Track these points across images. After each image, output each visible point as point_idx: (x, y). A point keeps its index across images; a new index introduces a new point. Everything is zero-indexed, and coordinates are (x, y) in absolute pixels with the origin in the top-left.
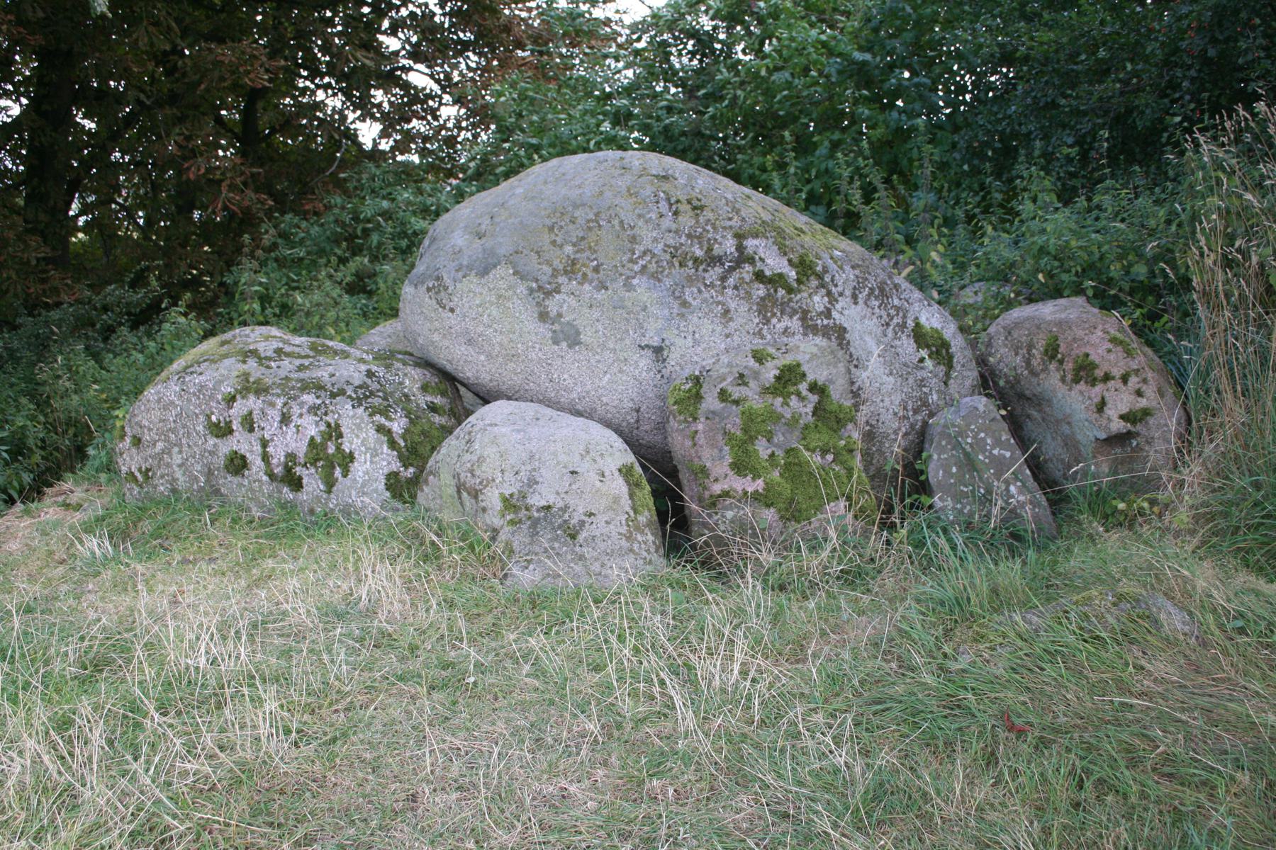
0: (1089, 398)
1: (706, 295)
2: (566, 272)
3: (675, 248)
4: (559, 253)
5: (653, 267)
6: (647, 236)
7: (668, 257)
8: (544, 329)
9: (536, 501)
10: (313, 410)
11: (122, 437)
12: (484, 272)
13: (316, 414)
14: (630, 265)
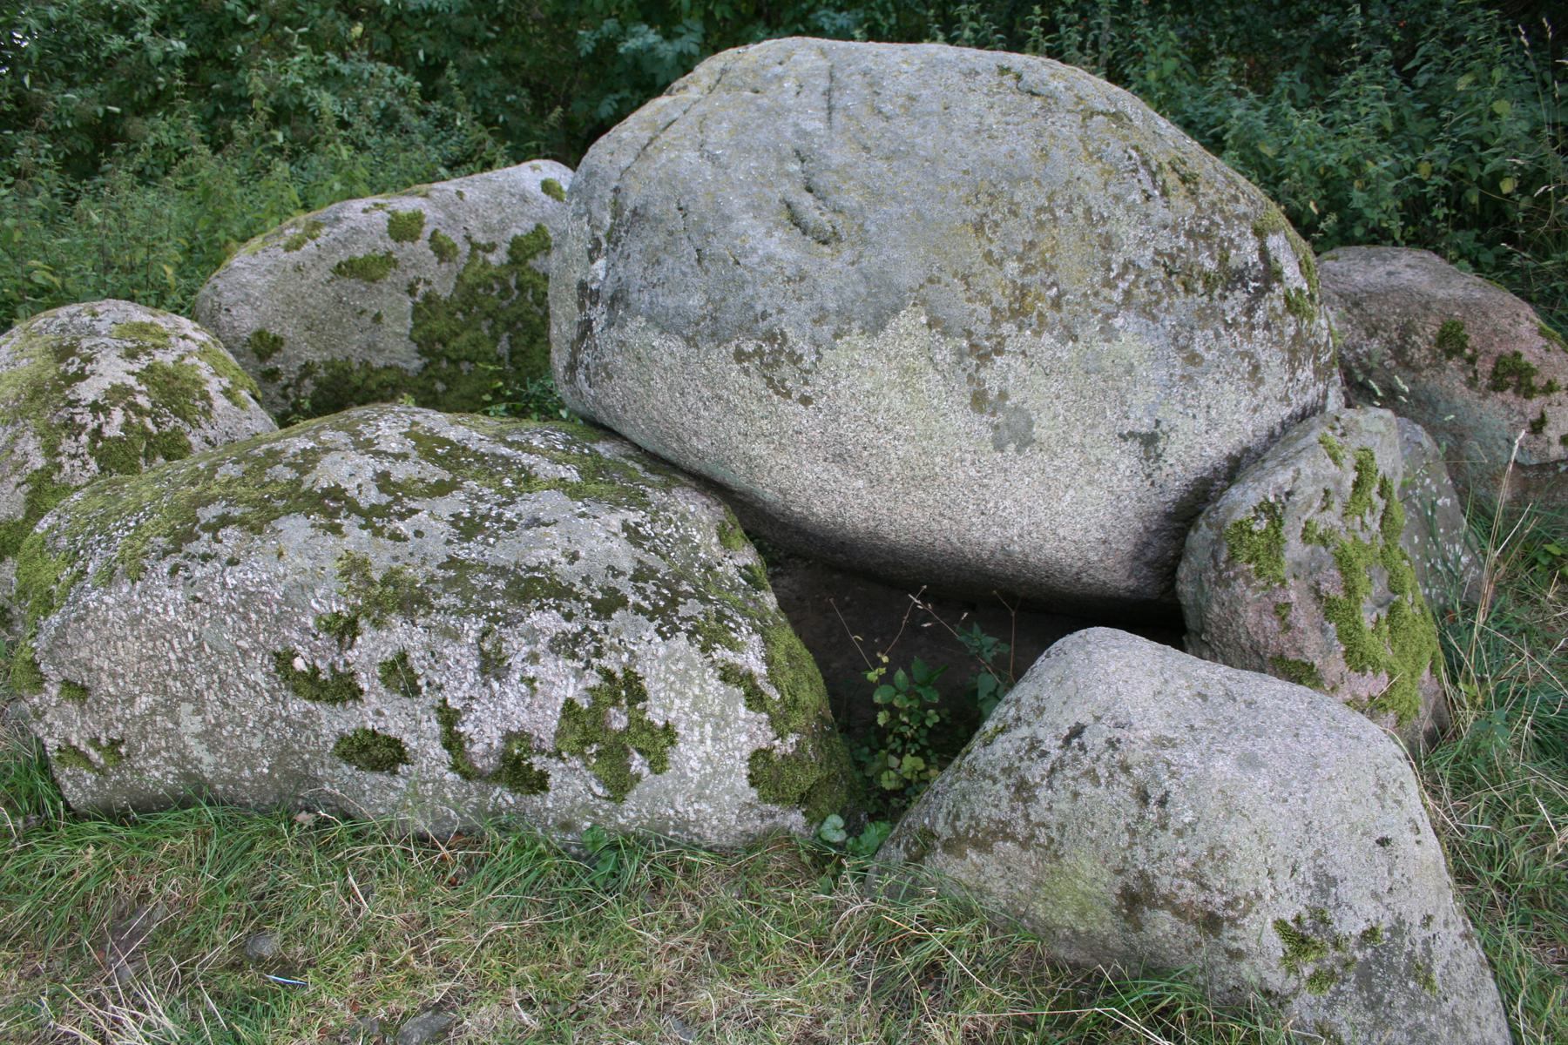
0: (1522, 413)
1: (1226, 342)
2: (1015, 314)
3: (1170, 256)
4: (999, 276)
5: (1141, 294)
6: (1128, 232)
7: (1162, 273)
8: (980, 425)
9: (1350, 925)
10: (565, 646)
11: (39, 684)
12: (876, 325)
13: (573, 656)
14: (1106, 292)
